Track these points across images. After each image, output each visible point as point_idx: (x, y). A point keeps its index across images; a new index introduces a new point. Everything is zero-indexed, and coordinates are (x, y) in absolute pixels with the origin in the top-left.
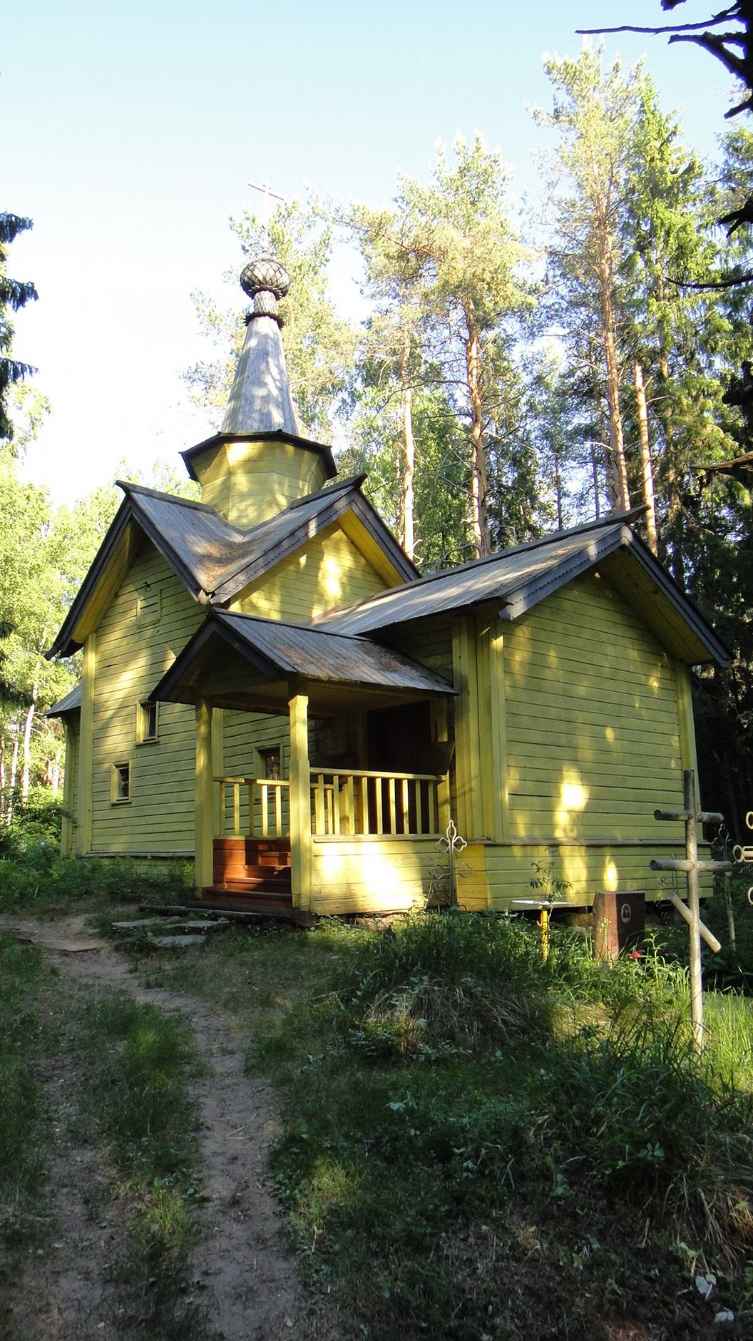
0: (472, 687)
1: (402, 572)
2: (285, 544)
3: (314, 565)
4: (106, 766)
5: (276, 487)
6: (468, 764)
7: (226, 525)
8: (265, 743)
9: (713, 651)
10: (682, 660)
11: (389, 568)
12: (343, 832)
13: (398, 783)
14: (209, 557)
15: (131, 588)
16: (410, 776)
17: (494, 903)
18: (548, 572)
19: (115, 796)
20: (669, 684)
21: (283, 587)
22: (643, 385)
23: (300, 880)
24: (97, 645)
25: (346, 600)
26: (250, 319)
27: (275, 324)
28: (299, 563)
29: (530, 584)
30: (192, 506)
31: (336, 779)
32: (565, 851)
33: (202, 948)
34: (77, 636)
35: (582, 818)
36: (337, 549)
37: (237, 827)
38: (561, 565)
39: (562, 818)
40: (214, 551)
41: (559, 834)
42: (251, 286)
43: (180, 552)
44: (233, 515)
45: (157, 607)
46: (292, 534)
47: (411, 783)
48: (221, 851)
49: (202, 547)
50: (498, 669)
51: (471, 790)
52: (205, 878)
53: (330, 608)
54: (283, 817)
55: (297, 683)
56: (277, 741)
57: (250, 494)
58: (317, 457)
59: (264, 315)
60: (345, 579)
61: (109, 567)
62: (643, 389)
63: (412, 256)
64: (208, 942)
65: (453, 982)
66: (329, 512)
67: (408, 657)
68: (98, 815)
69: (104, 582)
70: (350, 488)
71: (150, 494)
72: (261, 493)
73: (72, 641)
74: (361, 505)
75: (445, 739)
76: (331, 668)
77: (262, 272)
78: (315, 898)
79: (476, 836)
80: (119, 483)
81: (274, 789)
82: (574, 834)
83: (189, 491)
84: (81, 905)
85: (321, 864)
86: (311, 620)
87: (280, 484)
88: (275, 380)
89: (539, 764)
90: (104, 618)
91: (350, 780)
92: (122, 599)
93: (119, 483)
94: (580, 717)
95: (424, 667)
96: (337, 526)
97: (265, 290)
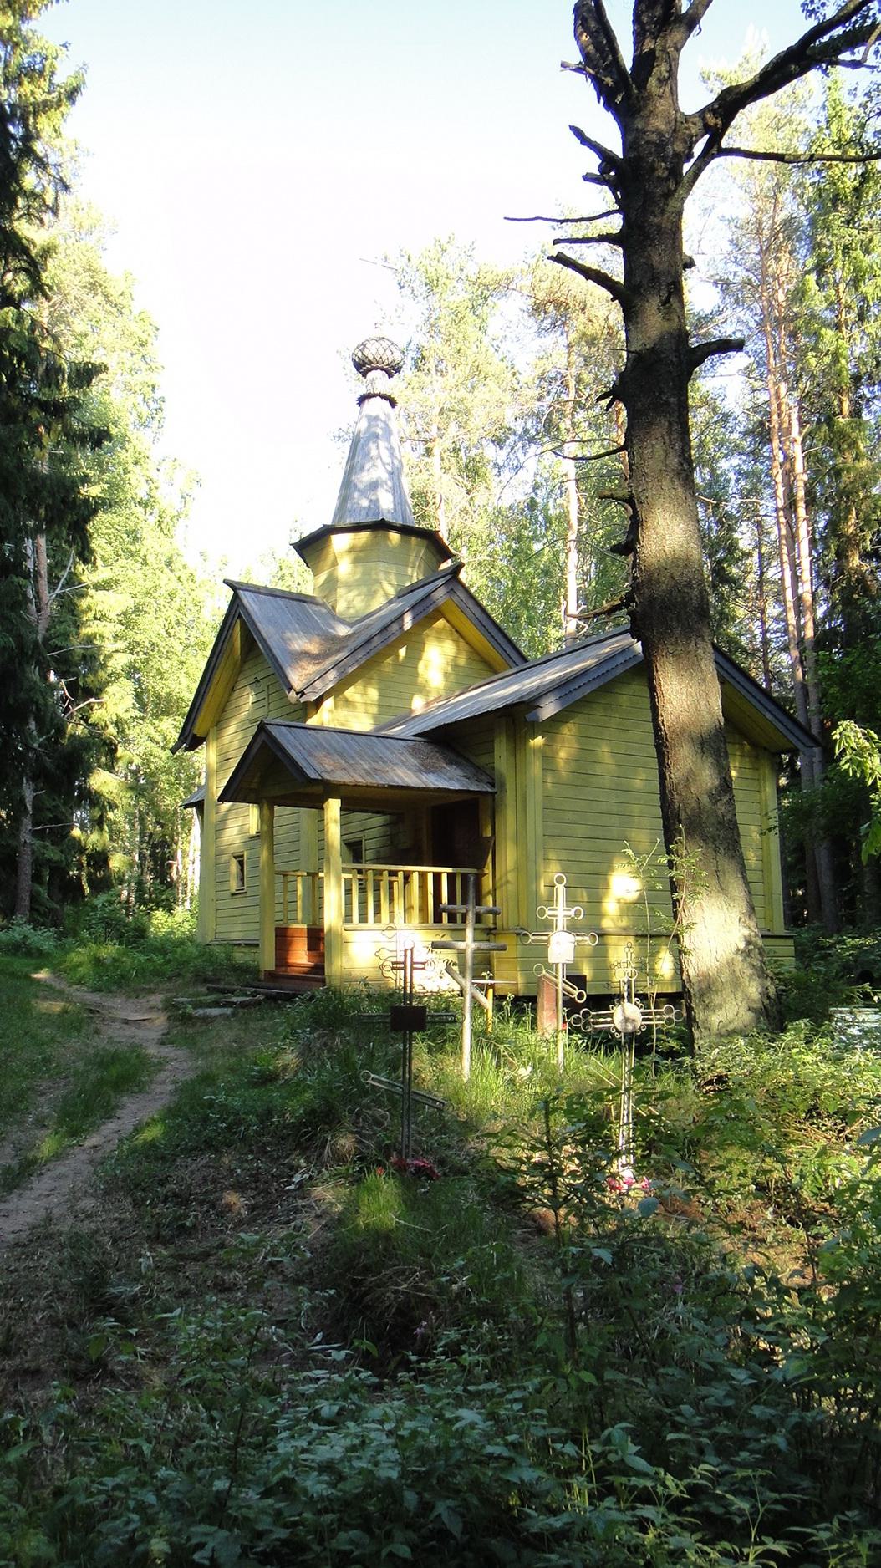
0: (509, 786)
1: (507, 658)
2: (376, 640)
3: (415, 655)
4: (224, 858)
5: (382, 576)
6: (508, 856)
7: (334, 617)
8: (351, 836)
9: (792, 739)
10: (765, 749)
11: (494, 655)
12: (378, 920)
13: (437, 877)
14: (306, 654)
15: (244, 682)
16: (450, 870)
17: (526, 987)
18: (584, 673)
19: (234, 886)
20: (748, 773)
21: (381, 680)
22: (800, 433)
23: (331, 964)
24: (218, 738)
25: (449, 692)
26: (362, 400)
27: (387, 403)
28: (398, 656)
29: (561, 687)
30: (301, 599)
31: (401, 875)
32: (612, 940)
33: (226, 1018)
34: (198, 731)
35: (632, 909)
36: (440, 639)
37: (300, 915)
38: (599, 665)
39: (610, 907)
40: (313, 648)
41: (607, 924)
42: (363, 366)
43: (276, 651)
44: (341, 607)
45: (264, 703)
46: (385, 628)
47: (451, 877)
48: (283, 938)
49: (300, 643)
50: (536, 767)
51: (507, 882)
52: (268, 962)
53: (431, 699)
54: (366, 908)
55: (332, 789)
56: (360, 835)
57: (357, 584)
58: (425, 542)
59: (375, 395)
60: (449, 669)
61: (223, 663)
62: (800, 439)
63: (551, 308)
64: (233, 1014)
65: (333, 1035)
66: (427, 603)
67: (460, 755)
68: (221, 904)
69: (221, 677)
70: (449, 577)
71: (256, 590)
72: (367, 584)
73: (195, 736)
74: (462, 595)
75: (489, 835)
76: (363, 773)
77: (370, 353)
78: (348, 978)
79: (511, 926)
80: (226, 582)
81: (381, 874)
82: (624, 923)
83: (305, 581)
84: (168, 985)
85: (352, 949)
86: (411, 711)
87: (386, 573)
88: (384, 465)
89: (584, 856)
90: (223, 711)
91: (415, 876)
92: (236, 693)
93: (226, 582)
94: (636, 809)
95: (472, 764)
96: (438, 614)
97: (376, 369)
